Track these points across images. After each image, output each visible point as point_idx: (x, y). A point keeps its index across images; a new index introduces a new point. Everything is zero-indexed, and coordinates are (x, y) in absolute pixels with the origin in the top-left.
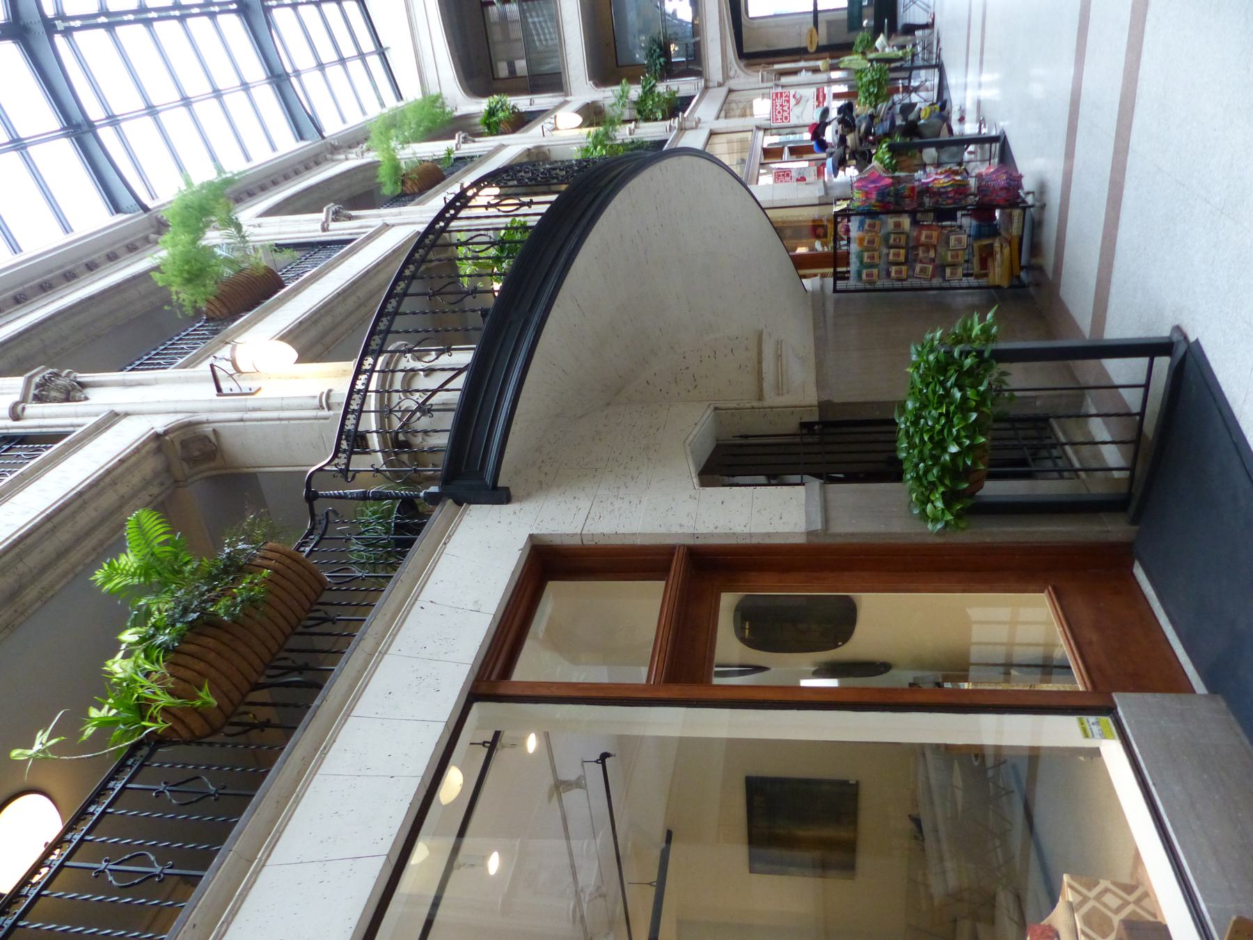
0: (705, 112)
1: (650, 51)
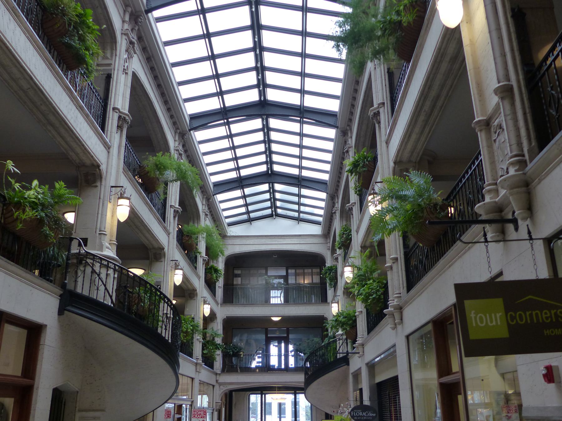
0: (205, 374)
1: (236, 347)
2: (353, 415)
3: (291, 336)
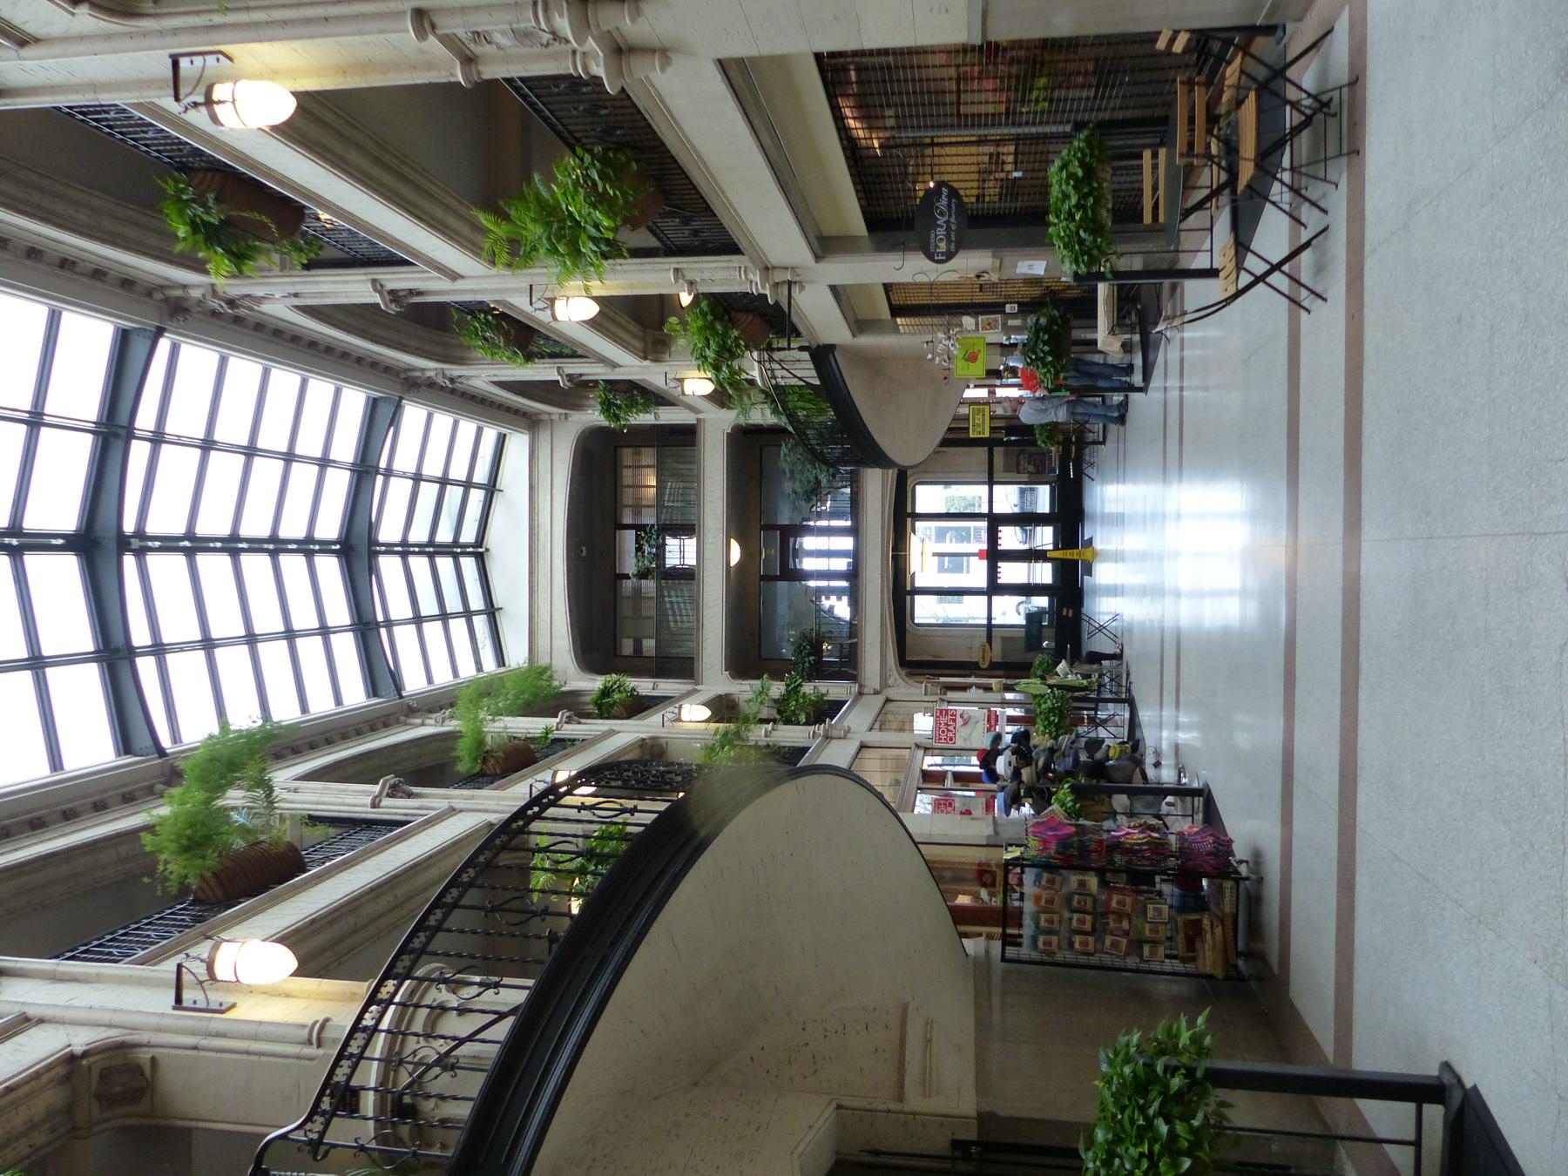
0: (856, 720)
2: (943, 254)
3: (784, 519)
